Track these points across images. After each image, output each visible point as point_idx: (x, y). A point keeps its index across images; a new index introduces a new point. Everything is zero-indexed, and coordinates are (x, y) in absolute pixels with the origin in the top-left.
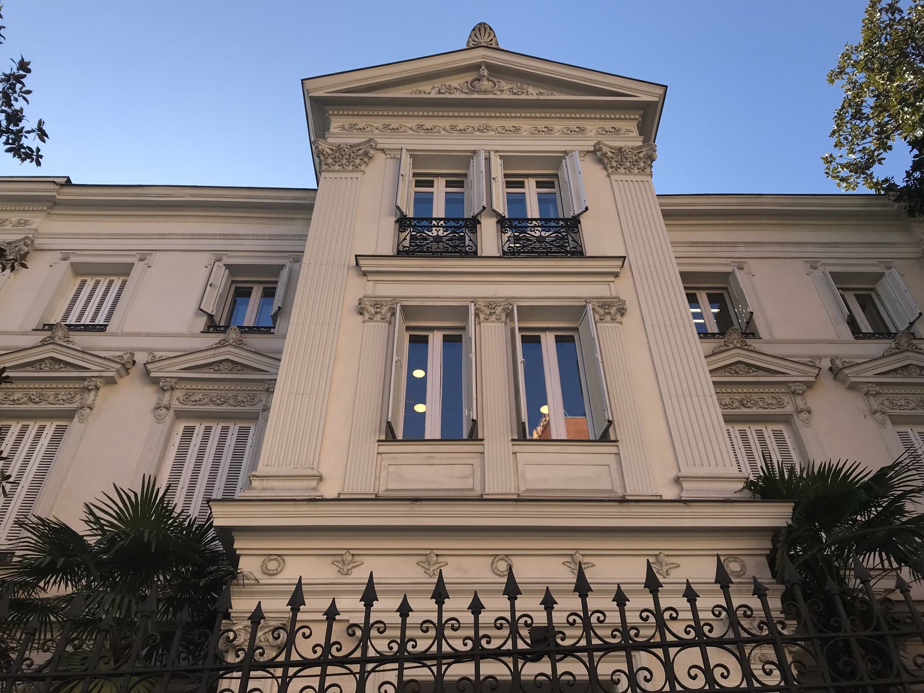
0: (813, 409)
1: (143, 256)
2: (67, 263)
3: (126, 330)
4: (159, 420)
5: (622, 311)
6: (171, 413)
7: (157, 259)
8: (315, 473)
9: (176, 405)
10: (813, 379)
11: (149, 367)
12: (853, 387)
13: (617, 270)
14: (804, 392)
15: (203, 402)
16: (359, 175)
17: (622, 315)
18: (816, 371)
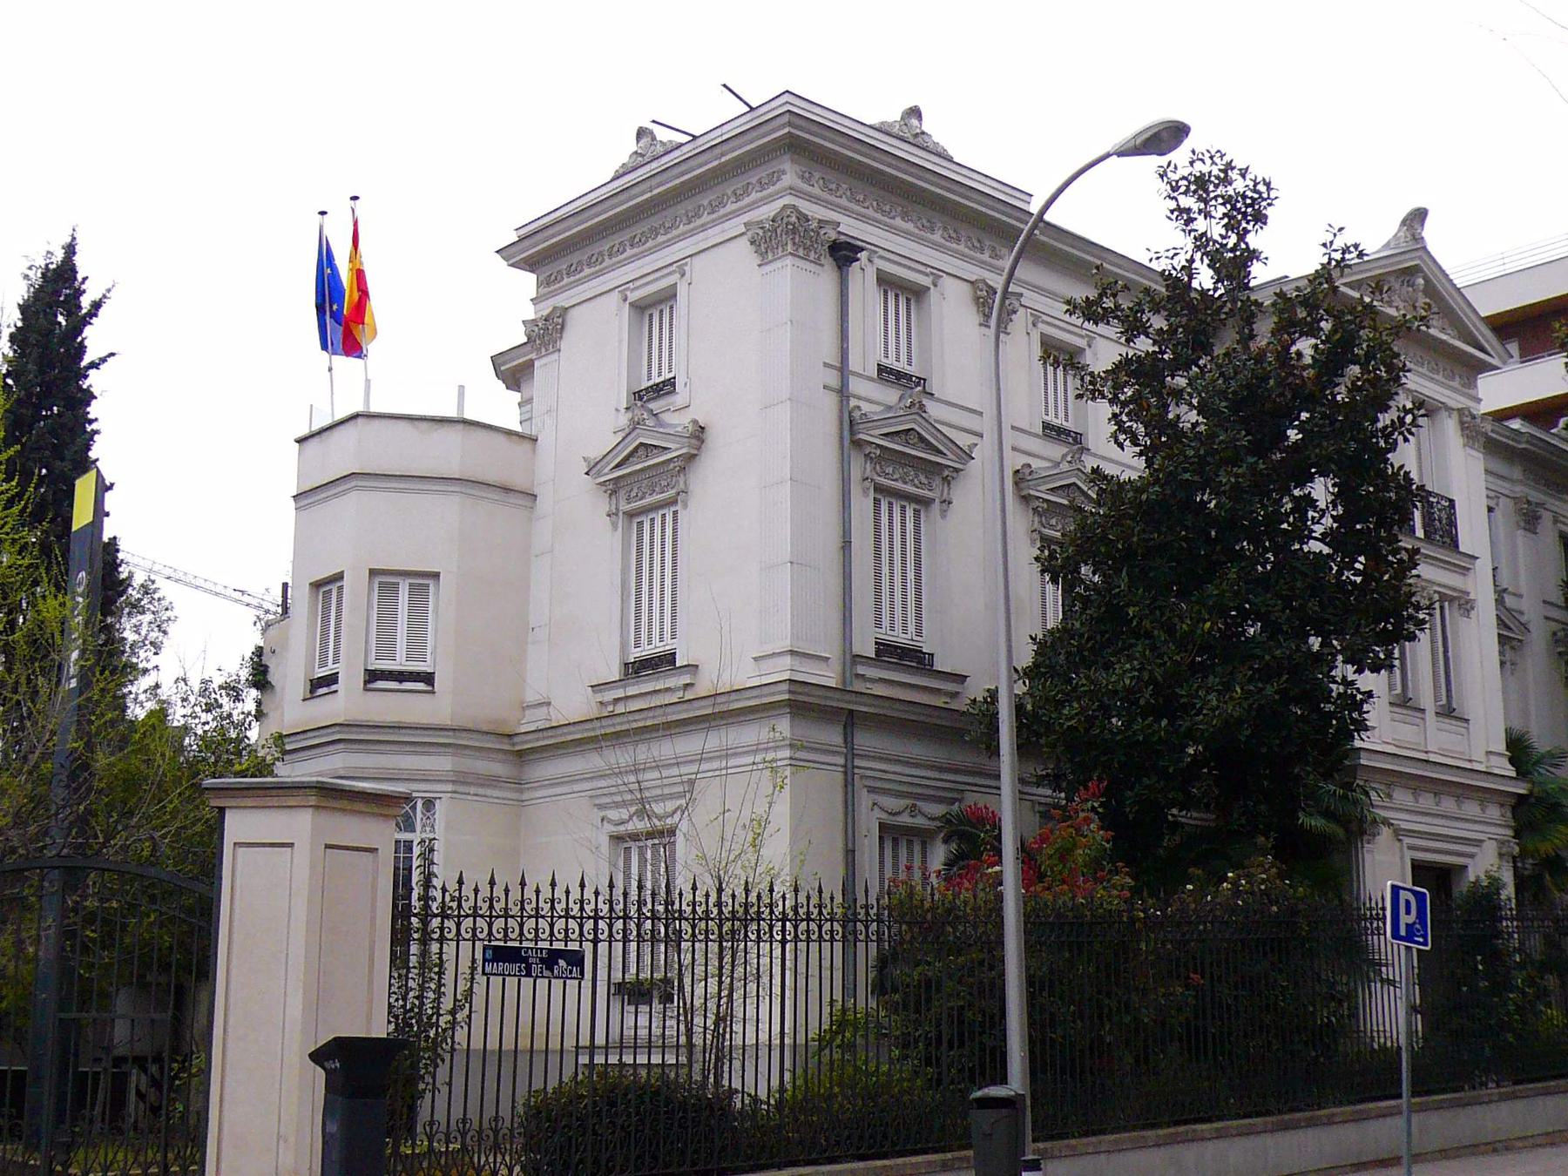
1: (680, 266)
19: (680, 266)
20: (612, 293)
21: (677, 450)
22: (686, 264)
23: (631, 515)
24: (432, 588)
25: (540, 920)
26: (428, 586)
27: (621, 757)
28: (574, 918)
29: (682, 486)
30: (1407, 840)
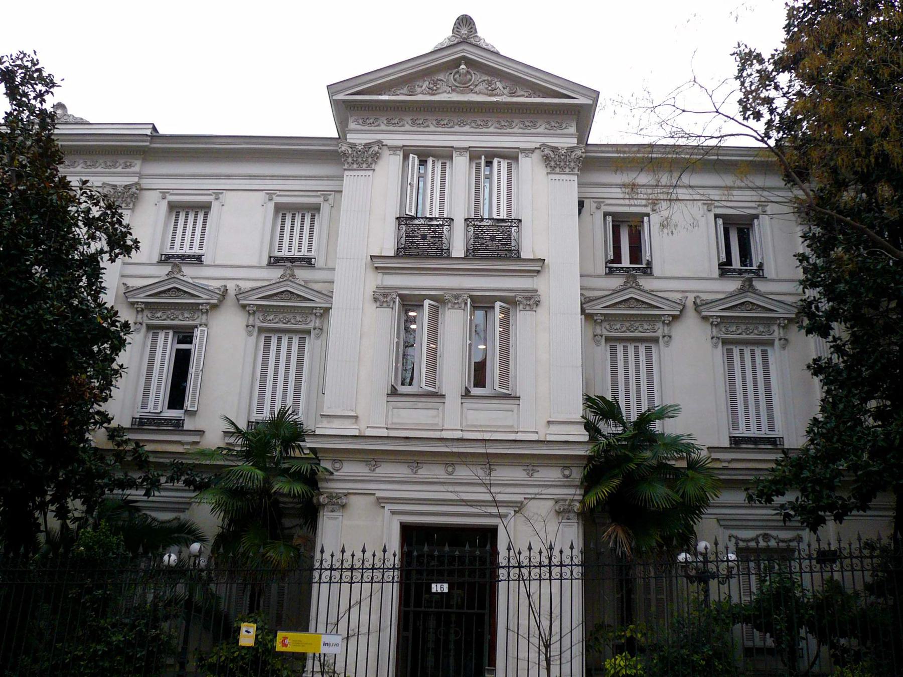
0: (673, 337)
1: (217, 194)
2: (166, 202)
3: (217, 263)
4: (250, 334)
5: (537, 303)
6: (256, 329)
7: (228, 197)
8: (353, 414)
9: (258, 324)
10: (678, 313)
11: (239, 297)
12: (705, 318)
13: (539, 268)
14: (670, 322)
15: (275, 321)
16: (370, 173)
17: (537, 305)
18: (681, 307)
19: (217, 194)
20: (261, 193)
21: (668, 310)
22: (330, 195)
23: (261, 330)
24: (307, 338)
25: (854, 559)
26: (271, 337)
27: (757, 473)
28: (856, 557)
29: (204, 321)
30: (388, 507)
